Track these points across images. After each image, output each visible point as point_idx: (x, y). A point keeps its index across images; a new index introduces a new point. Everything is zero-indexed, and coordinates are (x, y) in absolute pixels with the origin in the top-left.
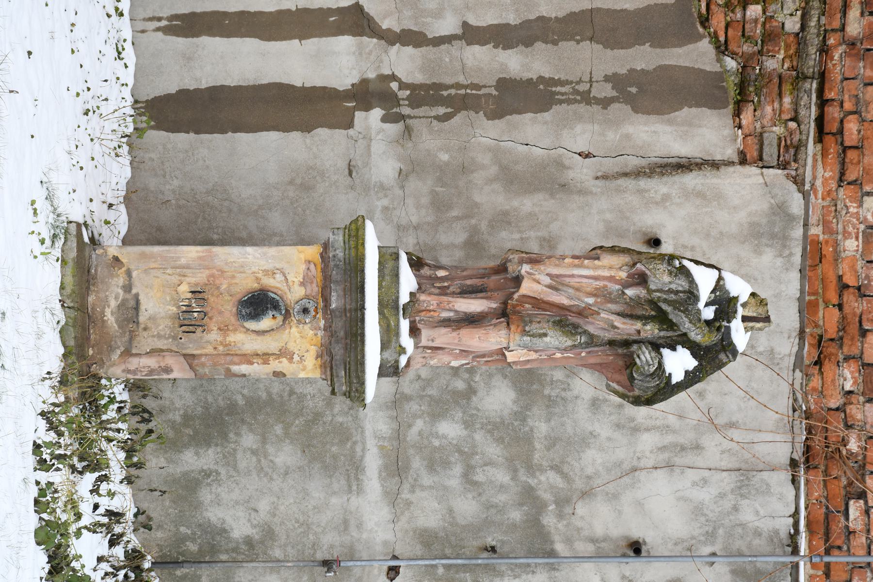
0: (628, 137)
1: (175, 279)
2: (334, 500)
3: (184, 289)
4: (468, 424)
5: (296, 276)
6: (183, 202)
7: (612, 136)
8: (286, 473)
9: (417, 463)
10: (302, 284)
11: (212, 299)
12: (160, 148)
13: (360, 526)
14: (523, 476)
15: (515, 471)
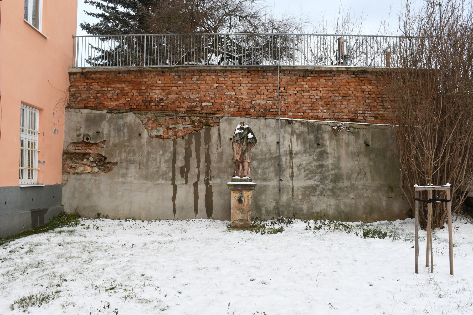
0: (214, 143)
2: (270, 189)
4: (259, 168)
5: (236, 195)
9: (265, 176)
13: (274, 186)
14: (267, 160)
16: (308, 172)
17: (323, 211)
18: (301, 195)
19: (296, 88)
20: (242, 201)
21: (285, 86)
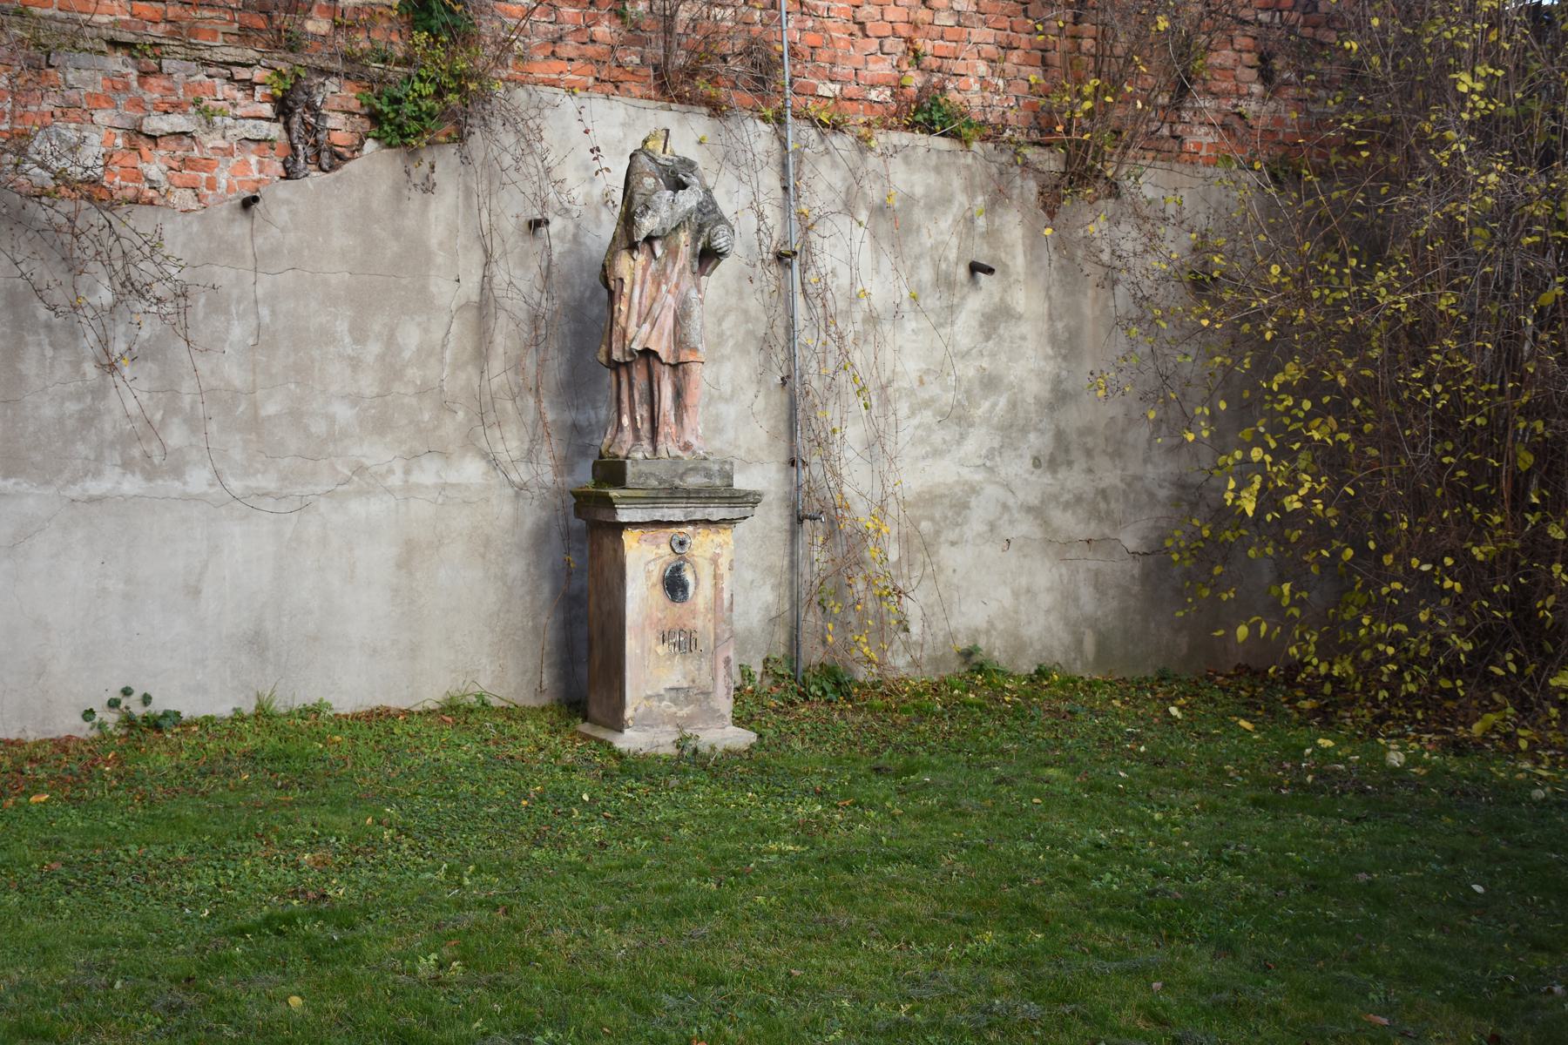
0: (441, 244)
3: (662, 650)
6: (501, 654)
7: (440, 258)
10: (658, 547)
11: (670, 625)
12: (454, 675)
14: (727, 349)
15: (723, 356)
16: (927, 416)
17: (1000, 626)
20: (684, 587)
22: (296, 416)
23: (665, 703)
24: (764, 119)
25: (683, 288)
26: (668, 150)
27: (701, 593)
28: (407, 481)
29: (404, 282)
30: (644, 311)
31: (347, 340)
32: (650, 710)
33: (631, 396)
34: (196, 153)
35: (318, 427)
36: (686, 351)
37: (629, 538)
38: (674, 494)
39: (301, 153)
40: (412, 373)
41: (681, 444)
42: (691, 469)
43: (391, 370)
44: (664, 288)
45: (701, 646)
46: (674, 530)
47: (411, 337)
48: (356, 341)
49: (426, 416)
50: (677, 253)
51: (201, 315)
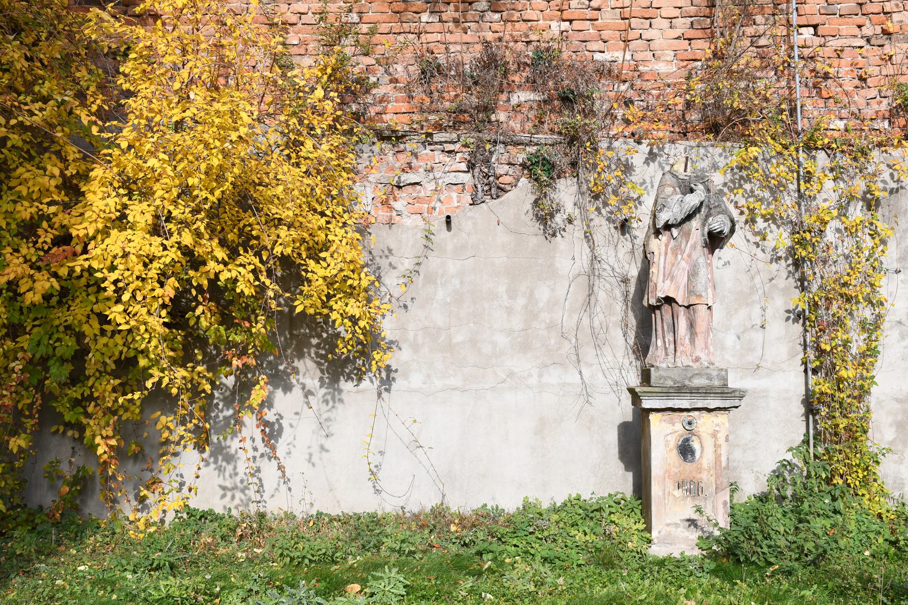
1: (671, 498)
3: (678, 493)
5: (669, 428)
8: (756, 433)
10: (673, 424)
18: (891, 425)
19: (860, 27)
20: (693, 452)
21: (817, 20)
22: (473, 342)
23: (679, 529)
24: (882, 263)
25: (694, 256)
26: (688, 170)
27: (705, 453)
28: (540, 382)
29: (540, 261)
30: (667, 272)
31: (505, 297)
32: (670, 534)
33: (663, 327)
34: (422, 194)
35: (487, 349)
36: (694, 297)
37: (653, 417)
38: (681, 390)
39: (480, 189)
40: (545, 316)
41: (694, 358)
42: (697, 374)
43: (531, 315)
44: (679, 257)
45: (705, 492)
46: (685, 414)
47: (543, 293)
48: (510, 297)
49: (553, 342)
50: (689, 234)
51: (420, 286)
